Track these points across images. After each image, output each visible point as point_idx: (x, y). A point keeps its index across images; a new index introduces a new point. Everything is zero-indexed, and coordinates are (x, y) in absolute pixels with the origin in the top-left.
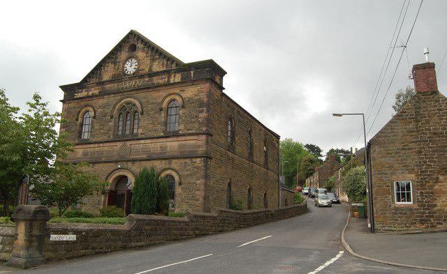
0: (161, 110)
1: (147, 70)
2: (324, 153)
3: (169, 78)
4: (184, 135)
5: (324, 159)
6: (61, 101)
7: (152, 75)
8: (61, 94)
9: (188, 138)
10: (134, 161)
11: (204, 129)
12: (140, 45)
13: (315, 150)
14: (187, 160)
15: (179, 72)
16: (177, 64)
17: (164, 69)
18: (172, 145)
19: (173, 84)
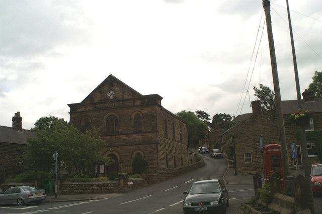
0: (131, 119)
1: (121, 97)
2: (211, 117)
3: (134, 102)
4: (145, 133)
5: (211, 121)
7: (124, 100)
8: (68, 109)
9: (147, 134)
10: (118, 146)
14: (147, 145)
17: (131, 97)
18: (139, 137)
19: (136, 106)
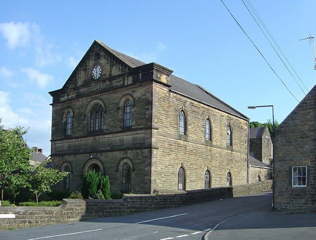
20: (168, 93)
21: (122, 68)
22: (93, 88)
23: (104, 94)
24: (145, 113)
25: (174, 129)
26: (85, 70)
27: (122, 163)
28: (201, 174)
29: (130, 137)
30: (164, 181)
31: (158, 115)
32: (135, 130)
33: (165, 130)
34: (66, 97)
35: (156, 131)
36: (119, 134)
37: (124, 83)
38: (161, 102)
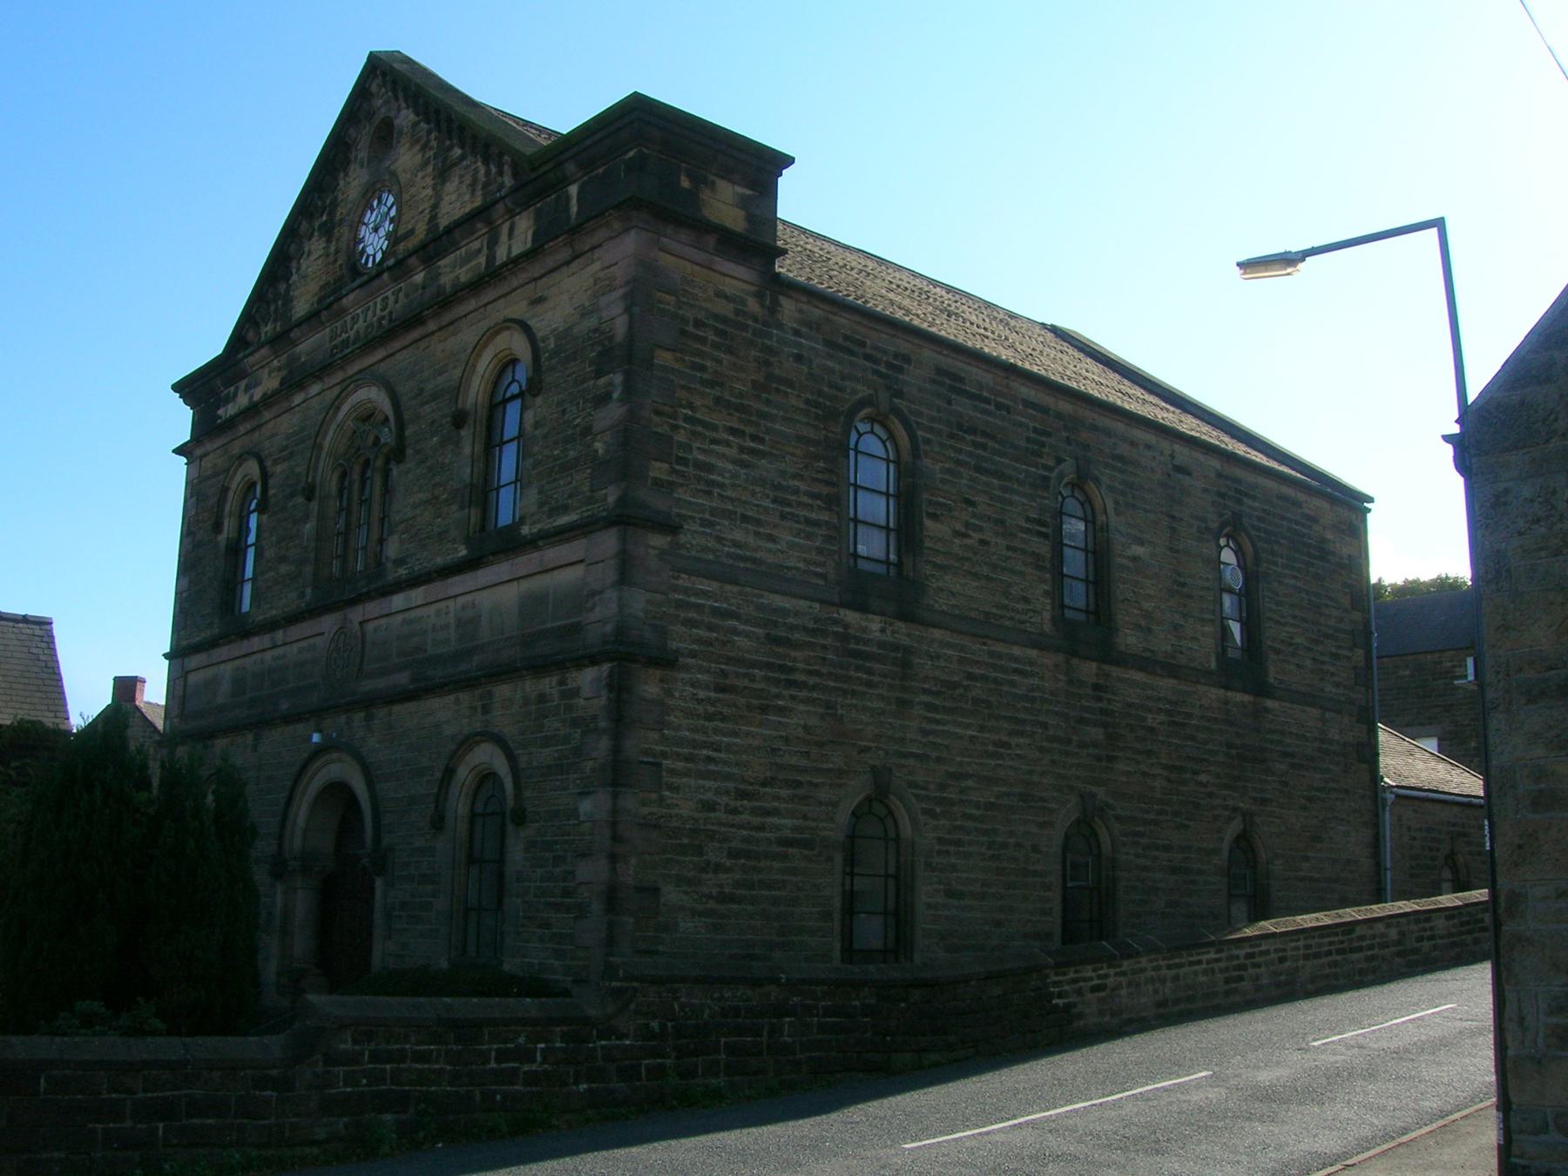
6: (179, 451)
11: (612, 495)
12: (405, 117)
13: (1447, 578)
15: (525, 206)
16: (515, 166)
20: (759, 296)
21: (488, 173)
22: (355, 320)
23: (397, 345)
24: (587, 430)
25: (808, 536)
26: (328, 231)
27: (463, 772)
28: (1035, 848)
29: (509, 595)
30: (724, 898)
31: (681, 437)
32: (532, 543)
33: (738, 535)
34: (243, 401)
35: (658, 541)
36: (457, 584)
37: (491, 257)
38: (700, 354)
